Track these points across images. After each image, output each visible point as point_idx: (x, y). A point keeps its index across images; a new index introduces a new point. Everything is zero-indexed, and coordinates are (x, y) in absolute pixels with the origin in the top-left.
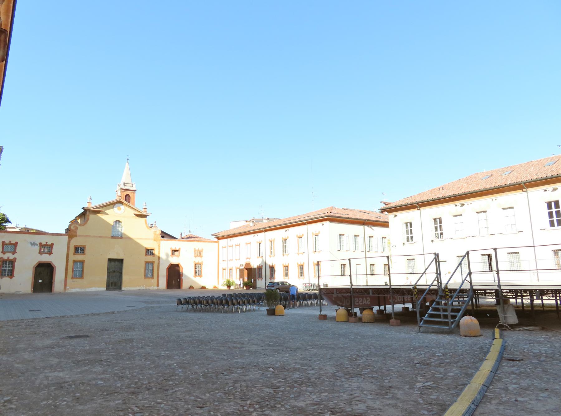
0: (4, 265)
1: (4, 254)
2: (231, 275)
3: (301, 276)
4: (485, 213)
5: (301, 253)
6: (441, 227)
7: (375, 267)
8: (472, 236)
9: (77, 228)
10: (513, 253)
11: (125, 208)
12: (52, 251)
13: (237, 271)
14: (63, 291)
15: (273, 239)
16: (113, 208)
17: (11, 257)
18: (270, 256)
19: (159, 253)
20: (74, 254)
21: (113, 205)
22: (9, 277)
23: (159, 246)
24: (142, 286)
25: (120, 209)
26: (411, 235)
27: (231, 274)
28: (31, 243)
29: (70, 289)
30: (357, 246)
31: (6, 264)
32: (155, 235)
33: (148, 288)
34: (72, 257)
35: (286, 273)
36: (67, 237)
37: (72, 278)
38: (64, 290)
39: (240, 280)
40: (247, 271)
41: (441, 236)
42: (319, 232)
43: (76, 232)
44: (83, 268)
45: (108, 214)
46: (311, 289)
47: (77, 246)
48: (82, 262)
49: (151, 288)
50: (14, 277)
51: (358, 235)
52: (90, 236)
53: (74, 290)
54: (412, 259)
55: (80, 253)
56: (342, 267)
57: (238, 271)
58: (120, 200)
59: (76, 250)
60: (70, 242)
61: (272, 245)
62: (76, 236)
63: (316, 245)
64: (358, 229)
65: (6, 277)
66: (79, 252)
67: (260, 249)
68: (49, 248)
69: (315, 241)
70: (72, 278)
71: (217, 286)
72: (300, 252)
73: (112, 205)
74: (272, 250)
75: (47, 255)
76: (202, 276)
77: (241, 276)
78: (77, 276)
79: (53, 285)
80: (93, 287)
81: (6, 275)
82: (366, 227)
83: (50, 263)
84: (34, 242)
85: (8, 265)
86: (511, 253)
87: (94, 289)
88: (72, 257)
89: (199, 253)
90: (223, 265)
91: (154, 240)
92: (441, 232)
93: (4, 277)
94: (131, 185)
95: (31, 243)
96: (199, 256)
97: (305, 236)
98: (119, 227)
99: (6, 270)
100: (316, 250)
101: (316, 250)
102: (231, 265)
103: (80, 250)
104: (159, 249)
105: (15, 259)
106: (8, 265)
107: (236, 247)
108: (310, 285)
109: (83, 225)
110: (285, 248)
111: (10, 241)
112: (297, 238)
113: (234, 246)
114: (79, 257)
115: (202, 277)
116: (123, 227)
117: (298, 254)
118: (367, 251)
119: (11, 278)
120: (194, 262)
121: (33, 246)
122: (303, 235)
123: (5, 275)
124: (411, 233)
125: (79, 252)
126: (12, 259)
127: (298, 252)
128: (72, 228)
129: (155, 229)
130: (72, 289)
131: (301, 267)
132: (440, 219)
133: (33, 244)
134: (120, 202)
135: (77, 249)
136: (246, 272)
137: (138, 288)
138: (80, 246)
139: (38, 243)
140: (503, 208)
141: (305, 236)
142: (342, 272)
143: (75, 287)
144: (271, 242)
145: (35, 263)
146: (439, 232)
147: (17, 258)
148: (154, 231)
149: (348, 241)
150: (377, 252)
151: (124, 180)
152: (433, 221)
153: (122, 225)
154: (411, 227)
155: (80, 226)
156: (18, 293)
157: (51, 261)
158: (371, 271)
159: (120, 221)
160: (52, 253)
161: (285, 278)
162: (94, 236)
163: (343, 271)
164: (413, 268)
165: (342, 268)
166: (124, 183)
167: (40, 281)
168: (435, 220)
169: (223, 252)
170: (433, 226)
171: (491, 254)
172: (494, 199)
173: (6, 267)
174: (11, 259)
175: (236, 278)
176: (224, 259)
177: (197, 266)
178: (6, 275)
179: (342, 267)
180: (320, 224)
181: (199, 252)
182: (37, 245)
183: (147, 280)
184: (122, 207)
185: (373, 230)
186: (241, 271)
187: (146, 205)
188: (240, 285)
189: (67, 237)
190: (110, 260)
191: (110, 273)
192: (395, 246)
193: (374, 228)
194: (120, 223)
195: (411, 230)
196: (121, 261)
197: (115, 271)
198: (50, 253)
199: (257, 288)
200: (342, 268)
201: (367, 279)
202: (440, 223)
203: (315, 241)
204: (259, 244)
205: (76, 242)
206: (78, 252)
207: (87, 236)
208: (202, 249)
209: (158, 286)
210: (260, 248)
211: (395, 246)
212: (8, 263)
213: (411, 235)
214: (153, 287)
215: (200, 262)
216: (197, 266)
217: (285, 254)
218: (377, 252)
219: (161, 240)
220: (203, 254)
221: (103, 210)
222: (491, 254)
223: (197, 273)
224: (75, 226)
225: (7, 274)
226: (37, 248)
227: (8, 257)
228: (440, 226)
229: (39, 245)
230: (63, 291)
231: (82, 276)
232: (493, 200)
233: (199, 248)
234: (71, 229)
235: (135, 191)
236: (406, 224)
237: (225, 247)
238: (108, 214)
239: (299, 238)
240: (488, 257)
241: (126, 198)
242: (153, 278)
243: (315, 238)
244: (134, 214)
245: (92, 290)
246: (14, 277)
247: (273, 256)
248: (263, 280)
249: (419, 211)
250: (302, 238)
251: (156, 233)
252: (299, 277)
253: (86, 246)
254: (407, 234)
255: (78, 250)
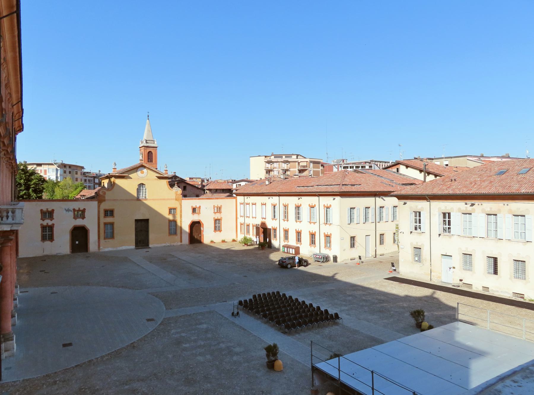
0: (45, 231)
1: (43, 220)
2: (248, 232)
3: (313, 243)
4: (495, 216)
5: (313, 223)
6: (449, 222)
7: (384, 237)
8: (480, 237)
9: (105, 193)
10: (519, 261)
11: (147, 171)
12: (84, 216)
13: (254, 229)
14: (98, 251)
15: (287, 204)
16: (137, 172)
17: (50, 223)
18: (284, 220)
19: (181, 224)
20: (104, 217)
21: (136, 169)
22: (50, 241)
23: (180, 205)
24: (167, 243)
25: (143, 173)
26: (420, 225)
27: (248, 230)
28: (65, 209)
29: (103, 249)
30: (368, 218)
31: (46, 230)
32: (176, 195)
33: (172, 244)
34: (103, 220)
35: (299, 238)
36: (97, 202)
37: (105, 239)
38: (98, 250)
39: (256, 238)
40: (263, 230)
41: (449, 230)
42: (330, 205)
43: (104, 197)
44: (113, 229)
45: (132, 178)
46: (321, 261)
47: (106, 210)
48: (112, 224)
49: (175, 244)
50: (54, 240)
51: (369, 207)
52: (117, 200)
53: (107, 250)
54: (419, 248)
55: (110, 215)
56: (352, 239)
57: (255, 228)
58: (143, 164)
59: (106, 213)
60: (100, 206)
61: (285, 210)
62: (104, 200)
63: (327, 217)
64: (369, 201)
65: (48, 241)
66: (109, 215)
67: (274, 211)
68: (81, 214)
69: (327, 213)
70: (105, 239)
71: (236, 240)
72: (311, 221)
73: (135, 169)
74: (286, 214)
75: (81, 219)
76: (221, 231)
77: (258, 234)
78: (108, 236)
79: (88, 247)
80: (123, 246)
81: (48, 239)
82: (377, 198)
83: (84, 227)
84: (68, 209)
85: (47, 230)
86: (517, 261)
87: (124, 248)
88: (103, 220)
89: (219, 210)
90: (241, 220)
91: (176, 200)
92: (449, 226)
93: (45, 241)
94: (153, 142)
95: (65, 209)
96: (218, 213)
97: (317, 206)
98: (143, 189)
99: (46, 234)
100: (327, 222)
101: (327, 222)
102: (248, 221)
103: (109, 213)
104: (181, 208)
105: (53, 224)
106: (47, 230)
107: (253, 205)
108: (320, 257)
109: (110, 190)
110: (298, 215)
111: (47, 209)
112: (309, 208)
113: (251, 204)
114: (109, 220)
115: (221, 232)
116: (147, 189)
117: (310, 223)
118: (377, 221)
119: (52, 242)
120: (214, 218)
121: (68, 212)
122: (315, 206)
123: (46, 239)
124: (420, 223)
125: (109, 215)
126: (50, 225)
127: (310, 221)
128: (101, 193)
129: (176, 189)
130: (105, 249)
131: (313, 235)
132: (449, 214)
133: (68, 210)
134: (142, 166)
135: (107, 212)
136: (261, 230)
137: (164, 245)
138: (109, 209)
139: (72, 209)
140: (514, 214)
141: (317, 206)
142: (351, 244)
143: (108, 247)
144: (285, 207)
145: (71, 227)
146: (447, 226)
147: (55, 224)
148: (175, 191)
149: (359, 214)
150: (388, 222)
151: (145, 137)
152: (442, 215)
153: (145, 187)
154: (420, 216)
155: (107, 191)
156: (59, 254)
157: (85, 225)
158: (380, 241)
159: (144, 183)
160: (85, 218)
161: (298, 244)
162: (121, 200)
163: (352, 243)
164: (419, 257)
165: (352, 240)
166: (146, 141)
167: (77, 242)
168: (444, 214)
169: (240, 208)
170: (442, 219)
171: (497, 258)
172: (506, 204)
173: (46, 232)
174: (50, 224)
175: (253, 235)
176: (242, 215)
177: (217, 221)
178: (48, 239)
179: (352, 239)
180: (331, 198)
181: (218, 208)
182: (71, 211)
183: (172, 237)
184: (145, 170)
185: (384, 200)
186: (257, 228)
187: (167, 167)
188: (257, 242)
189: (97, 202)
190: (137, 221)
191: (138, 232)
192: (403, 233)
193: (384, 198)
194: (144, 186)
195: (420, 220)
196: (147, 221)
197: (142, 230)
198: (83, 217)
199: (272, 248)
200: (352, 240)
201: (376, 249)
202: (449, 217)
203: (327, 213)
204: (274, 206)
205: (105, 206)
206: (108, 215)
207: (114, 200)
208: (221, 206)
209: (181, 242)
210: (275, 210)
211: (403, 233)
212: (47, 229)
213: (420, 225)
214: (177, 243)
215: (219, 218)
216: (217, 221)
217: (298, 220)
218: (388, 222)
219: (183, 199)
220: (223, 210)
221: (127, 175)
222: (497, 258)
223: (217, 228)
224: (103, 191)
225: (47, 238)
226: (71, 214)
227: (47, 224)
228: (449, 221)
229: (73, 211)
230: (98, 251)
231: (112, 237)
232: (504, 205)
233: (218, 205)
234: (100, 194)
235: (156, 147)
236: (416, 212)
237: (243, 204)
238: (132, 178)
239: (311, 207)
240: (494, 260)
241: (149, 154)
242: (177, 235)
243: (327, 210)
244: (156, 177)
245: (122, 248)
246: (54, 240)
247: (286, 220)
248: (277, 241)
249: (429, 202)
250: (314, 208)
251: (178, 193)
252: (310, 245)
253: (114, 209)
254: (416, 222)
255: (108, 213)
